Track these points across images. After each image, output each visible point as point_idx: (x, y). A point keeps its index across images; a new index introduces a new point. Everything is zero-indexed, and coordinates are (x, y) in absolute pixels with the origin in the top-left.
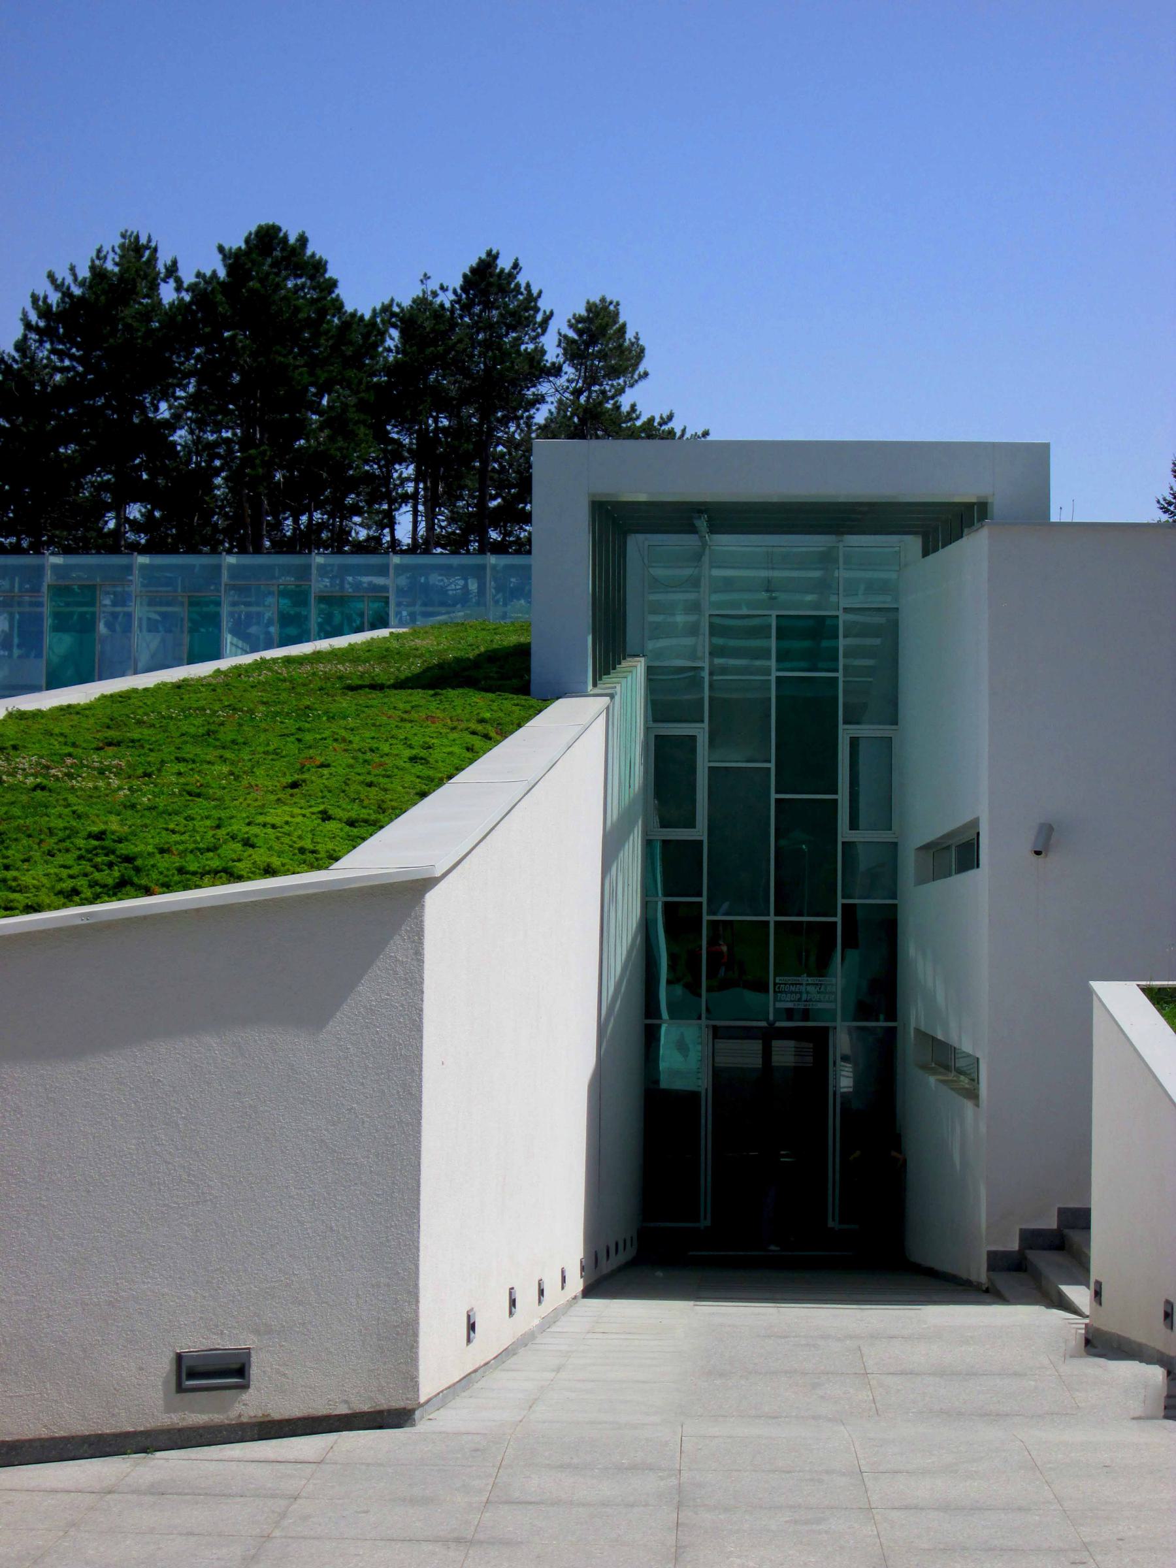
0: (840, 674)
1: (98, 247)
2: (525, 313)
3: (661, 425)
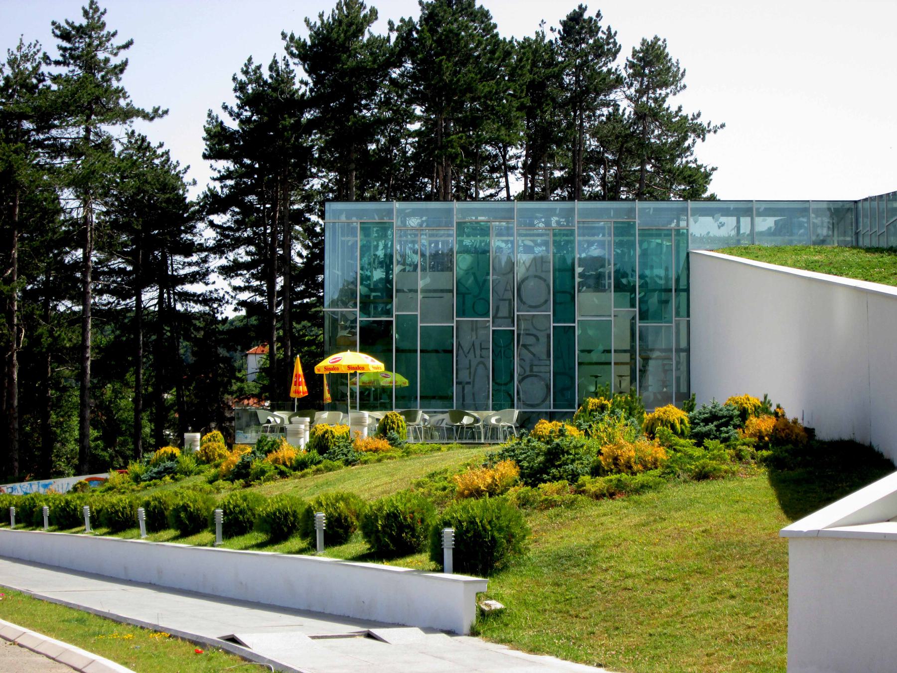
0: (576, 325)
1: (82, 12)
2: (606, 48)
3: (692, 120)
